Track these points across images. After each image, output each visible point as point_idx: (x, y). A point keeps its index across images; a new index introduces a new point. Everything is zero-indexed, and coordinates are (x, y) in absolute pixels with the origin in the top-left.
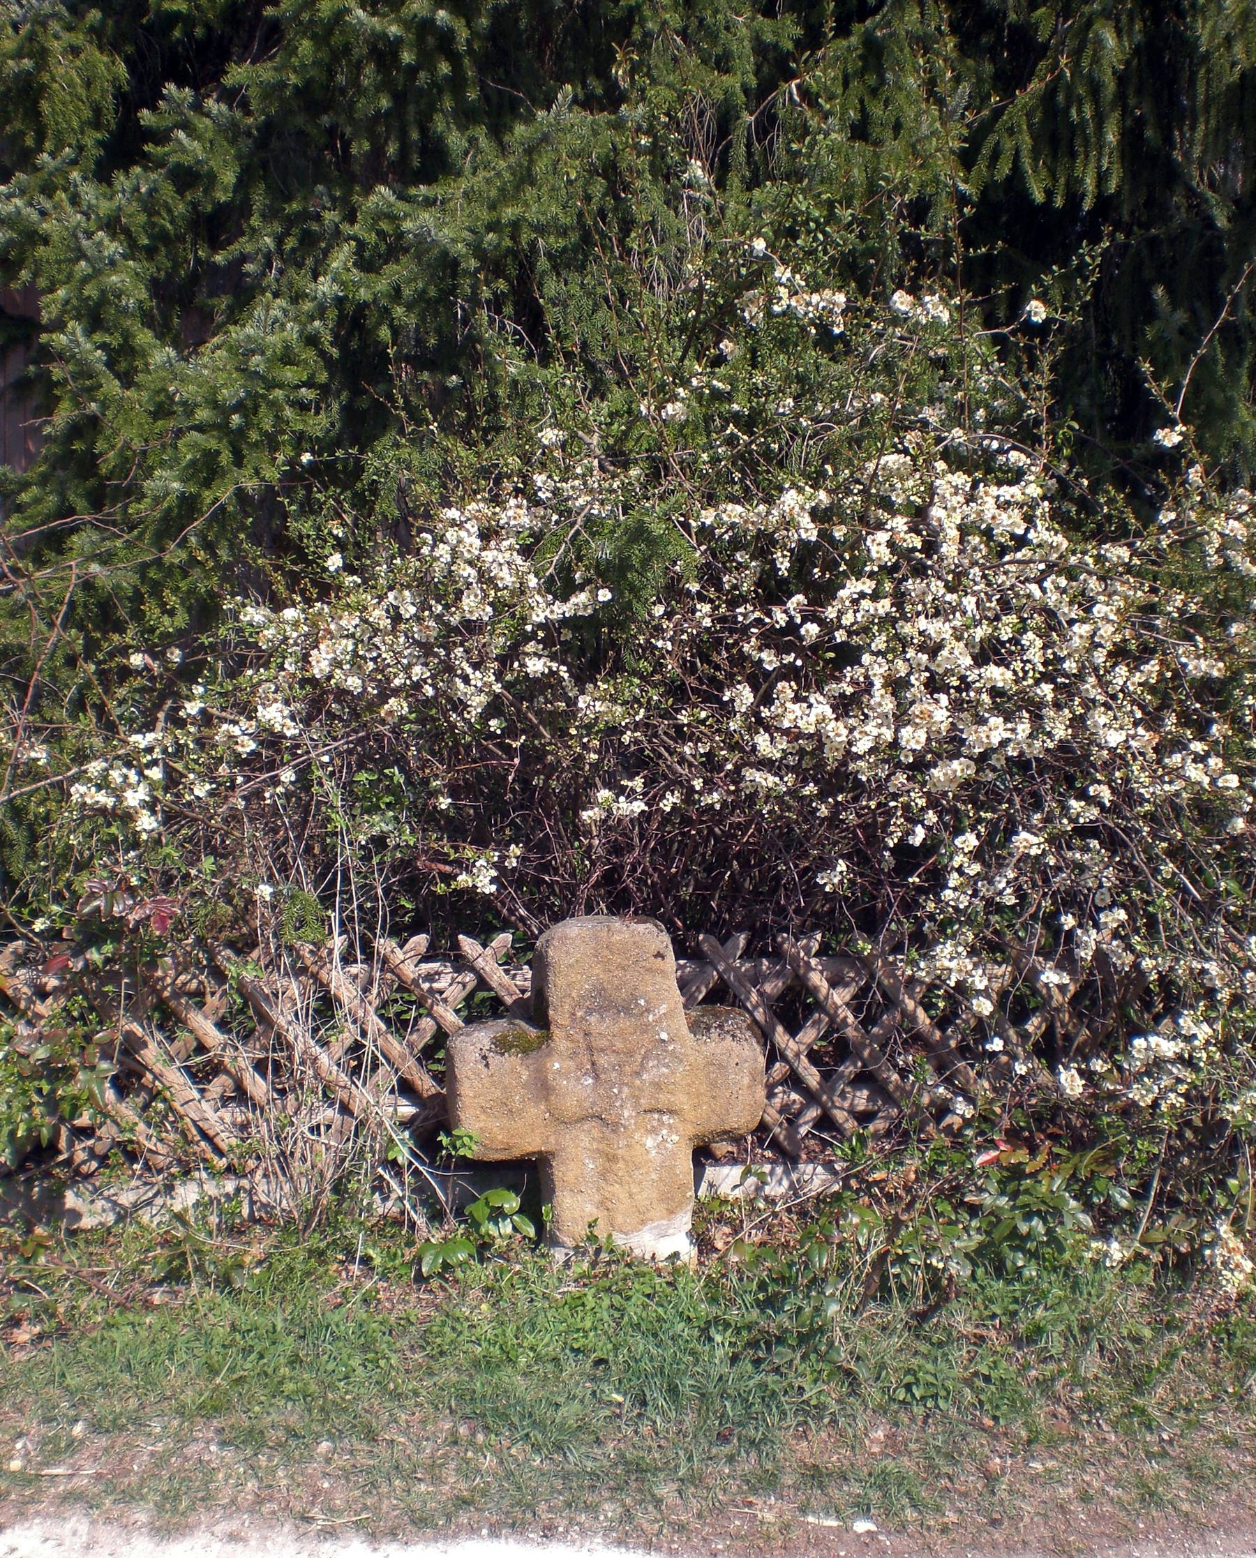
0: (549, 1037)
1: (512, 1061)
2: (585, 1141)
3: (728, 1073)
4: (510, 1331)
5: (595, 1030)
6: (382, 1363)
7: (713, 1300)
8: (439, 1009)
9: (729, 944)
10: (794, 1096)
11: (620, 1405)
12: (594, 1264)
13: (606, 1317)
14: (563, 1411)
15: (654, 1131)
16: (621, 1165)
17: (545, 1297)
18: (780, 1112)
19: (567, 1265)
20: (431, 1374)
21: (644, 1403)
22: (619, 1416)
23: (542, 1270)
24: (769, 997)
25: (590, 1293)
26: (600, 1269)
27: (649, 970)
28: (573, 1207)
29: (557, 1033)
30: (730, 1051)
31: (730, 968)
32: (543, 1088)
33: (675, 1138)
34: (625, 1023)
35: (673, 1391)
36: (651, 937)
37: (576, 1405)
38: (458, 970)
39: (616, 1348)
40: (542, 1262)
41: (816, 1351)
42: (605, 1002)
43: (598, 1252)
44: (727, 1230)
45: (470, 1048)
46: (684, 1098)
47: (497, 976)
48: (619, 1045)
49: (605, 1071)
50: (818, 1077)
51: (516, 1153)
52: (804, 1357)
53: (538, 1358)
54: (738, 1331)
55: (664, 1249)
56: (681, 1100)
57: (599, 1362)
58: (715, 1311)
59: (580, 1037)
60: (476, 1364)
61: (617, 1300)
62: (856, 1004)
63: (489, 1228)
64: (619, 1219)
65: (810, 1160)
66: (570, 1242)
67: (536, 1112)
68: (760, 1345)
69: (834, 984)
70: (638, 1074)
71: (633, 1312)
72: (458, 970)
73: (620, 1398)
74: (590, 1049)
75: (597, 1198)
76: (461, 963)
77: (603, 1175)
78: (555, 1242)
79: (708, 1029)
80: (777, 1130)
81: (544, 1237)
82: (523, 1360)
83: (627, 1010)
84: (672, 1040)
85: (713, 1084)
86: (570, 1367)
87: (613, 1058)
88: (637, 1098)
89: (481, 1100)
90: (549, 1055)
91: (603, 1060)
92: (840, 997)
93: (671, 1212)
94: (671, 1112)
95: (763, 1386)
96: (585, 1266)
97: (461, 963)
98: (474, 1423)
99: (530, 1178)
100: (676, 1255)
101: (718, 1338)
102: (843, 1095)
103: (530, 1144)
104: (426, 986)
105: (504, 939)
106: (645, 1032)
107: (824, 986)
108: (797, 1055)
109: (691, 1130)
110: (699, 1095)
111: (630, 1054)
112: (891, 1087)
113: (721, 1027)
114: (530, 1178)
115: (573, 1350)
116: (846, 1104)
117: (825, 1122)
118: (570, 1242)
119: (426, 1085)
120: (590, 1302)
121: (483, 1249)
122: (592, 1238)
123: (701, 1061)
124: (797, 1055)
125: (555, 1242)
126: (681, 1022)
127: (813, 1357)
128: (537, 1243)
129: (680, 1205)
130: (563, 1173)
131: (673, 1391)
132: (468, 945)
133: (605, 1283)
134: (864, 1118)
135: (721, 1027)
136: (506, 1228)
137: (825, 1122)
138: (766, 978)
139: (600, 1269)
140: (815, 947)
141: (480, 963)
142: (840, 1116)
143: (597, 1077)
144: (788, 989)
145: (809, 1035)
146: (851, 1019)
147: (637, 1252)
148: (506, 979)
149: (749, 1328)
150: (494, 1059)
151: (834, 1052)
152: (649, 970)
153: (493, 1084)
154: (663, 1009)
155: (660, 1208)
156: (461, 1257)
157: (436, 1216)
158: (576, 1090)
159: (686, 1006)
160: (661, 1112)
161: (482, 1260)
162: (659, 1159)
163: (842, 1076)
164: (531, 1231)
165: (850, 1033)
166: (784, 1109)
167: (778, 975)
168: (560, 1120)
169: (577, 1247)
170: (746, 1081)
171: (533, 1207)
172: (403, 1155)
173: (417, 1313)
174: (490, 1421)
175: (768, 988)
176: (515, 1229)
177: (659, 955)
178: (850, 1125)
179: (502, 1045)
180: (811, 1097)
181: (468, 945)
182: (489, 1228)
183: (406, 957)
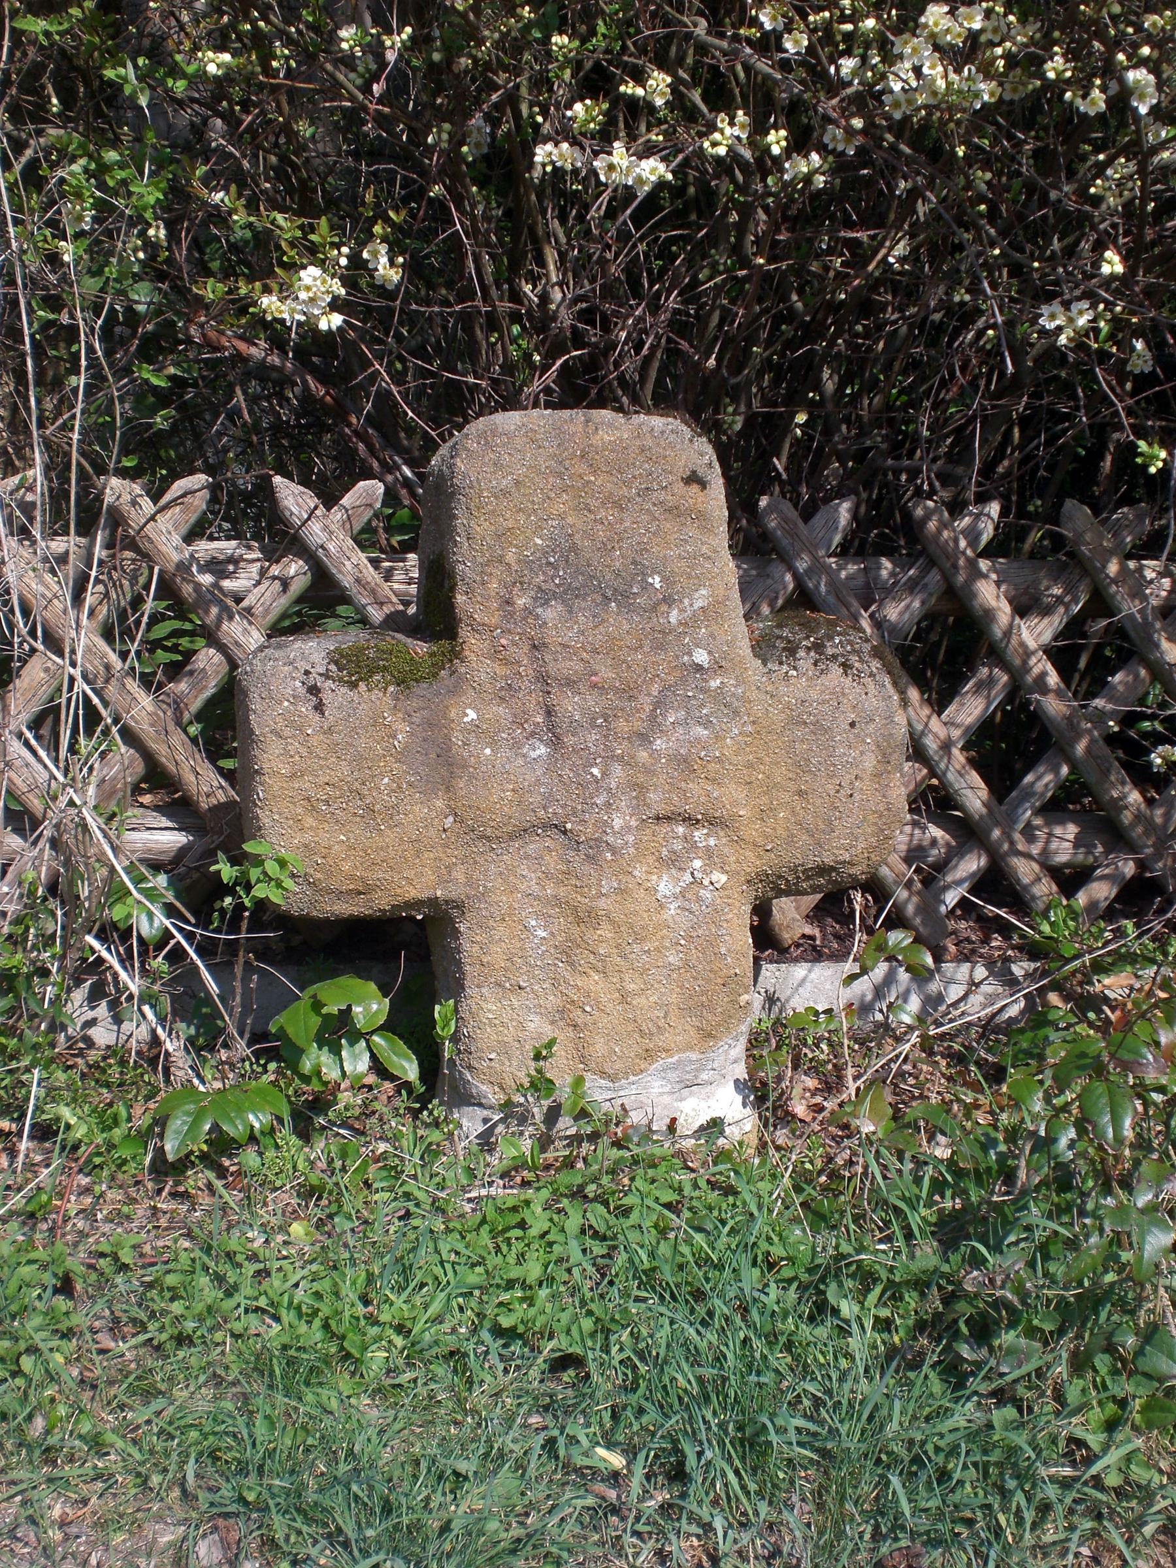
0: (455, 654)
1: (376, 699)
2: (529, 879)
3: (838, 746)
4: (350, 1285)
5: (552, 637)
6: (27, 1363)
7: (818, 1218)
8: (234, 629)
9: (818, 520)
10: (935, 832)
11: (615, 1477)
12: (544, 1142)
13: (576, 1255)
14: (473, 1499)
15: (674, 862)
16: (605, 931)
17: (438, 1208)
18: (908, 860)
19: (486, 1142)
20: (149, 1394)
21: (678, 1475)
22: (615, 1510)
23: (431, 1153)
24: (893, 629)
25: (539, 1197)
26: (558, 1151)
27: (674, 511)
28: (500, 1020)
29: (472, 642)
30: (839, 696)
31: (818, 568)
32: (442, 763)
33: (720, 878)
34: (618, 623)
35: (751, 1444)
36: (673, 444)
37: (505, 1480)
38: (272, 556)
39: (604, 1330)
40: (435, 1136)
41: (1110, 1349)
42: (577, 578)
43: (553, 1115)
44: (811, 1083)
45: (285, 679)
46: (740, 794)
47: (352, 565)
48: (606, 673)
49: (575, 728)
50: (984, 793)
51: (381, 902)
52: (1080, 1363)
53: (414, 1354)
54: (893, 1292)
55: (694, 1111)
56: (733, 797)
57: (563, 1362)
58: (828, 1243)
59: (521, 652)
60: (260, 1367)
61: (598, 1216)
62: (1061, 654)
63: (317, 1059)
64: (599, 1047)
65: (966, 957)
66: (493, 1096)
67: (424, 813)
68: (951, 1333)
69: (1022, 609)
70: (644, 738)
71: (638, 1242)
72: (272, 556)
73: (617, 1461)
74: (543, 679)
75: (553, 1001)
76: (280, 538)
77: (567, 953)
78: (464, 1098)
79: (792, 650)
80: (902, 894)
81: (439, 1082)
82: (377, 1357)
83: (624, 597)
84: (718, 668)
85: (802, 766)
86: (491, 1376)
87: (592, 701)
88: (641, 789)
89: (305, 784)
90: (454, 691)
91: (570, 705)
92: (1036, 633)
93: (708, 1035)
94: (712, 822)
95: (980, 1434)
96: (526, 1145)
97: (280, 538)
98: (238, 1529)
99: (409, 952)
100: (715, 1126)
101: (847, 1308)
102: (1029, 833)
103: (410, 883)
104: (206, 579)
105: (367, 492)
106: (659, 647)
107: (1004, 611)
108: (946, 746)
109: (752, 862)
110: (770, 787)
111: (629, 692)
112: (1127, 817)
113: (818, 647)
114: (409, 952)
115: (498, 1331)
116: (1035, 850)
117: (995, 883)
118: (493, 1096)
119: (205, 783)
120: (538, 1220)
121: (309, 1114)
122: (541, 1085)
123: (777, 716)
124: (946, 746)
125: (464, 1098)
126: (737, 633)
127: (1102, 1362)
128: (424, 1101)
129: (726, 1022)
130: (479, 946)
131: (751, 1444)
132: (293, 498)
133: (566, 1179)
134: (1070, 880)
135: (818, 647)
136: (357, 1062)
137: (995, 883)
138: (889, 592)
139: (558, 1151)
140: (987, 532)
141: (315, 533)
142: (1025, 870)
143: (556, 742)
144: (930, 618)
145: (970, 709)
146: (1053, 679)
147: (635, 1117)
148: (371, 574)
149: (920, 1284)
150: (336, 696)
151: (1009, 745)
152: (674, 511)
153: (333, 748)
154: (701, 597)
155: (682, 1030)
156: (257, 1121)
157: (206, 1040)
158: (512, 768)
159: (747, 617)
160: (690, 821)
161: (305, 1133)
162: (684, 921)
163: (1028, 794)
164: (410, 1070)
165: (1054, 707)
166: (914, 855)
167: (912, 586)
168: (478, 834)
169: (508, 1105)
170: (870, 762)
171: (412, 1024)
172: (150, 921)
173: (127, 1240)
174: (279, 1525)
175: (893, 612)
176: (379, 1068)
177: (694, 479)
178: (1044, 889)
179: (353, 668)
180: (968, 833)
181: (293, 498)
182: (317, 1059)
183: (166, 522)
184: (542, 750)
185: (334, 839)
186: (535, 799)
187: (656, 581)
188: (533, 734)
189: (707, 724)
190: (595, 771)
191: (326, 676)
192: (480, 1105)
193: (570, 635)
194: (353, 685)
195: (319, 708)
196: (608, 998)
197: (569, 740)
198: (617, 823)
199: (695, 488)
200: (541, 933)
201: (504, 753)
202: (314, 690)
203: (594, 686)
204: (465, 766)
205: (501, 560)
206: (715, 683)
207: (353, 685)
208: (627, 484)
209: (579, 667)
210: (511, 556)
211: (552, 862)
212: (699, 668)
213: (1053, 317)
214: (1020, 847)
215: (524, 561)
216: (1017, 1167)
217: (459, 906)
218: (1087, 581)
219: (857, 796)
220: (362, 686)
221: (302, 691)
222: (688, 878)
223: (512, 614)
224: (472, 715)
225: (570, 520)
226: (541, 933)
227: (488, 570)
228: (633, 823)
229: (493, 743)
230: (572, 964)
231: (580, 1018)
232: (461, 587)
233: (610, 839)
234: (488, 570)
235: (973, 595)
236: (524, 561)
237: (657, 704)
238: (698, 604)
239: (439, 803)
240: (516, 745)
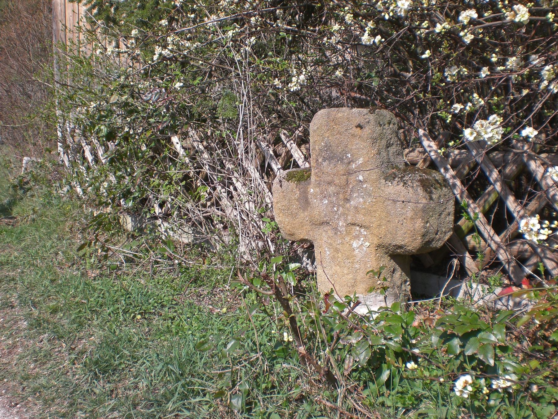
32: (305, 202)
83: (342, 159)
150: (285, 183)
152: (353, 135)
186: (323, 215)
187: (349, 155)
188: (325, 197)
194: (288, 181)
195: (281, 186)
198: (340, 224)
199: (359, 129)
200: (328, 253)
206: (365, 186)
207: (288, 181)
212: (361, 181)
214: (548, 256)
219: (404, 224)
224: (312, 190)
228: (344, 225)
235: (529, 165)
240: (321, 200)
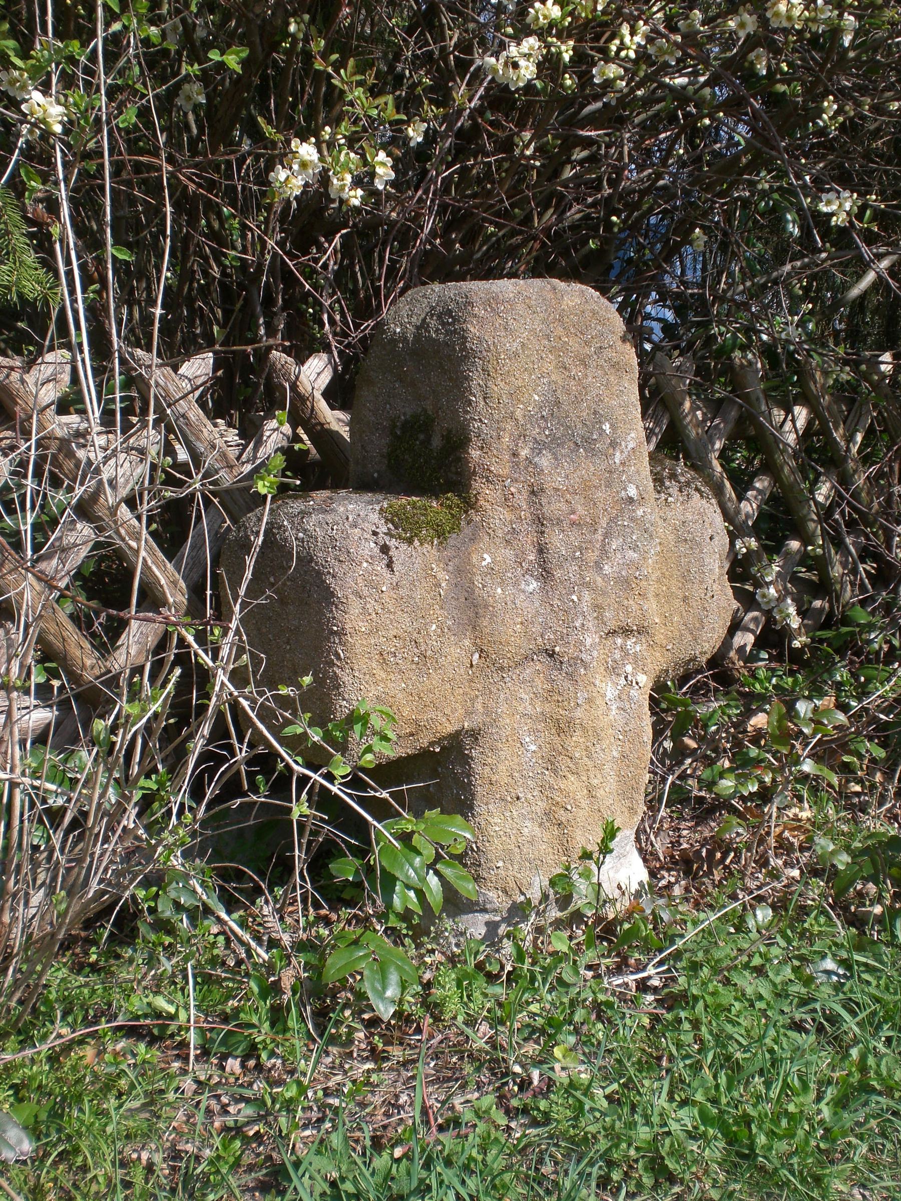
0: (469, 504)
29: (486, 493)
59: (522, 499)
74: (539, 521)
91: (557, 540)
150: (400, 551)
184: (534, 585)
185: (396, 687)
186: (536, 629)
187: (607, 427)
189: (635, 548)
190: (575, 598)
191: (389, 534)
192: (484, 910)
193: (559, 481)
195: (390, 565)
196: (581, 795)
197: (558, 574)
198: (589, 641)
201: (510, 590)
202: (385, 549)
203: (573, 523)
204: (486, 606)
205: (512, 416)
208: (587, 343)
209: (564, 507)
210: (519, 414)
211: (540, 684)
212: (631, 500)
213: (829, 202)
215: (529, 417)
216: (229, 912)
217: (475, 735)
218: (667, 416)
220: (416, 543)
221: (377, 550)
222: (623, 681)
223: (517, 464)
225: (553, 377)
226: (533, 748)
227: (502, 425)
229: (502, 583)
230: (555, 771)
231: (562, 815)
232: (475, 442)
233: (583, 656)
234: (502, 425)
236: (529, 417)
237: (606, 535)
238: (631, 445)
239: (467, 642)
